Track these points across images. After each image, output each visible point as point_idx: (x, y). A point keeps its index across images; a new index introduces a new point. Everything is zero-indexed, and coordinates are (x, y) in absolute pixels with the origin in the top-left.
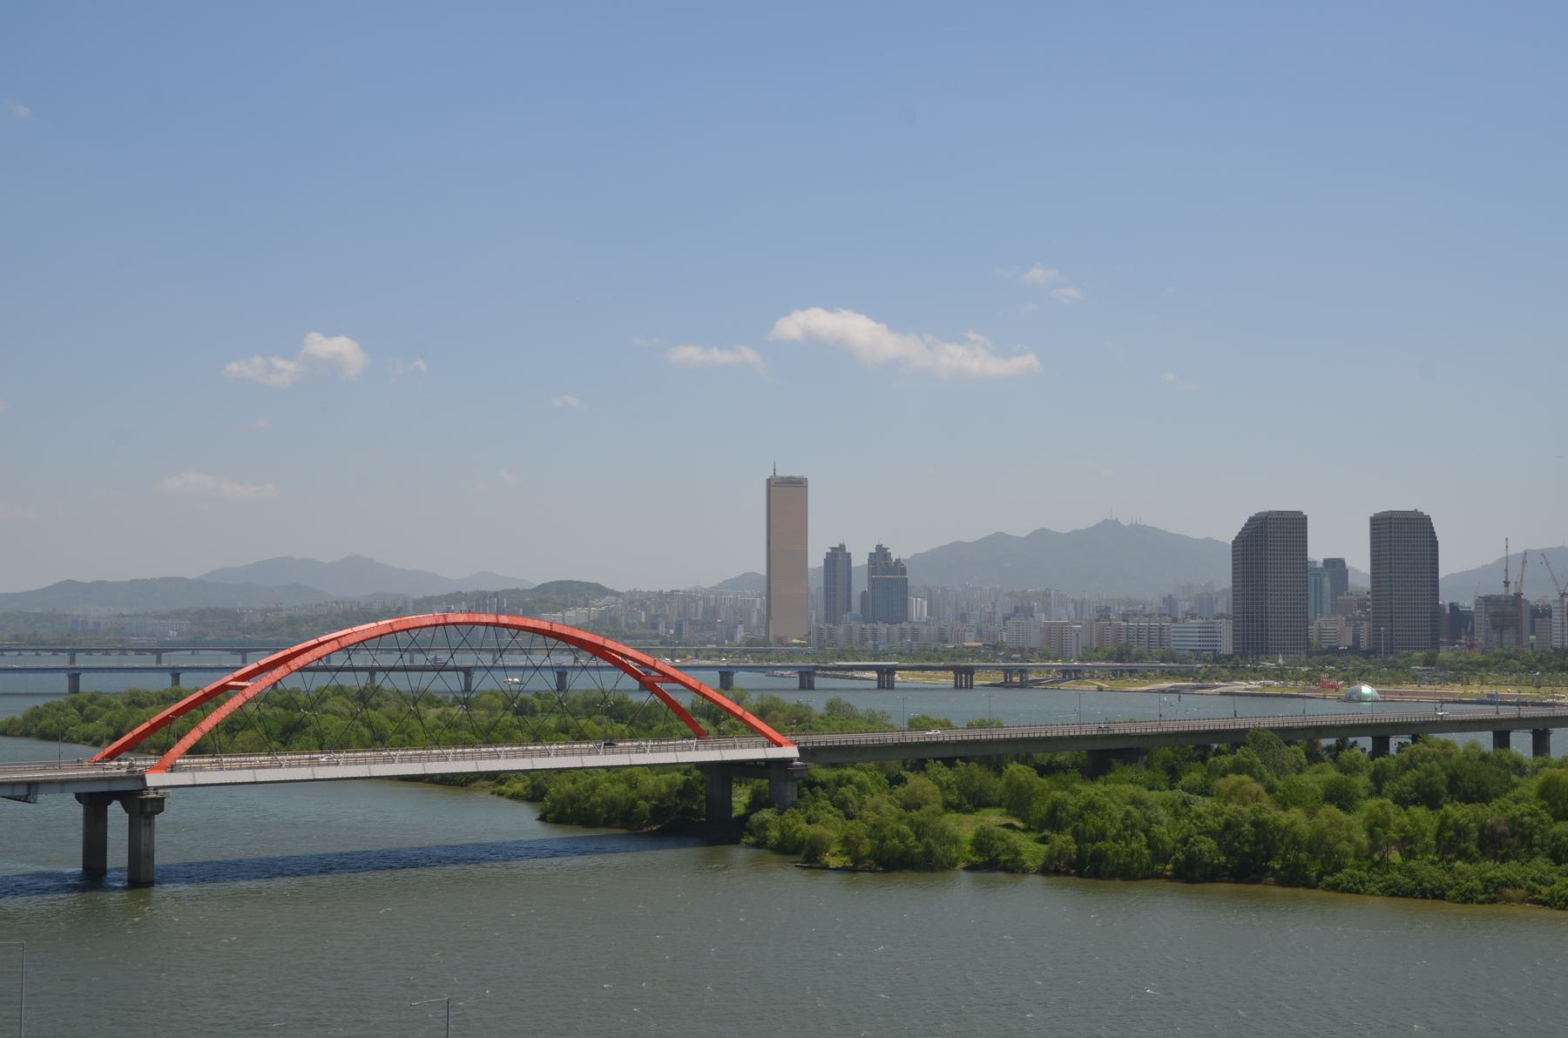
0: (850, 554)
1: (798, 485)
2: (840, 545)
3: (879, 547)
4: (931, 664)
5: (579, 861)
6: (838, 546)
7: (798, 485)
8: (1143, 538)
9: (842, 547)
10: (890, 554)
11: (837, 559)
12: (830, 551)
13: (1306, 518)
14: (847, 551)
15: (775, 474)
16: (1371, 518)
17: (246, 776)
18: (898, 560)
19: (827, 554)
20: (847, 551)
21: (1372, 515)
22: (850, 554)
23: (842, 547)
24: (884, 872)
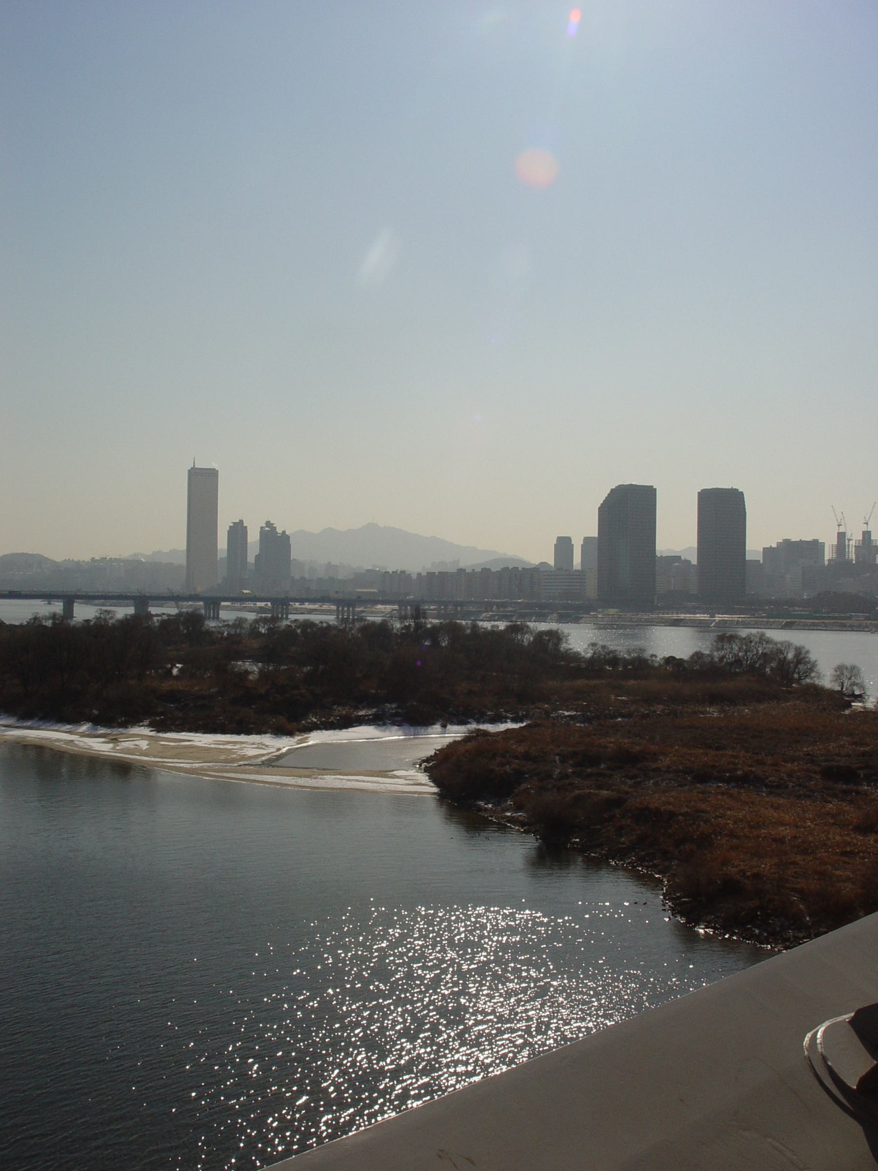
0: (246, 527)
1: (211, 475)
2: (240, 520)
3: (268, 524)
4: (836, 615)
5: (751, 967)
6: (238, 521)
7: (211, 475)
8: (40, 560)
9: (241, 522)
10: (276, 528)
11: (238, 531)
12: (232, 525)
13: (655, 489)
14: (245, 525)
15: (194, 466)
16: (699, 493)
17: (127, 756)
18: (284, 532)
19: (230, 527)
20: (245, 525)
21: (700, 491)
22: (246, 527)
23: (241, 522)
24: (614, 871)
